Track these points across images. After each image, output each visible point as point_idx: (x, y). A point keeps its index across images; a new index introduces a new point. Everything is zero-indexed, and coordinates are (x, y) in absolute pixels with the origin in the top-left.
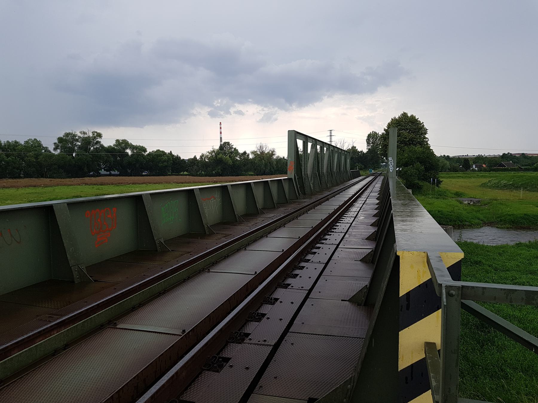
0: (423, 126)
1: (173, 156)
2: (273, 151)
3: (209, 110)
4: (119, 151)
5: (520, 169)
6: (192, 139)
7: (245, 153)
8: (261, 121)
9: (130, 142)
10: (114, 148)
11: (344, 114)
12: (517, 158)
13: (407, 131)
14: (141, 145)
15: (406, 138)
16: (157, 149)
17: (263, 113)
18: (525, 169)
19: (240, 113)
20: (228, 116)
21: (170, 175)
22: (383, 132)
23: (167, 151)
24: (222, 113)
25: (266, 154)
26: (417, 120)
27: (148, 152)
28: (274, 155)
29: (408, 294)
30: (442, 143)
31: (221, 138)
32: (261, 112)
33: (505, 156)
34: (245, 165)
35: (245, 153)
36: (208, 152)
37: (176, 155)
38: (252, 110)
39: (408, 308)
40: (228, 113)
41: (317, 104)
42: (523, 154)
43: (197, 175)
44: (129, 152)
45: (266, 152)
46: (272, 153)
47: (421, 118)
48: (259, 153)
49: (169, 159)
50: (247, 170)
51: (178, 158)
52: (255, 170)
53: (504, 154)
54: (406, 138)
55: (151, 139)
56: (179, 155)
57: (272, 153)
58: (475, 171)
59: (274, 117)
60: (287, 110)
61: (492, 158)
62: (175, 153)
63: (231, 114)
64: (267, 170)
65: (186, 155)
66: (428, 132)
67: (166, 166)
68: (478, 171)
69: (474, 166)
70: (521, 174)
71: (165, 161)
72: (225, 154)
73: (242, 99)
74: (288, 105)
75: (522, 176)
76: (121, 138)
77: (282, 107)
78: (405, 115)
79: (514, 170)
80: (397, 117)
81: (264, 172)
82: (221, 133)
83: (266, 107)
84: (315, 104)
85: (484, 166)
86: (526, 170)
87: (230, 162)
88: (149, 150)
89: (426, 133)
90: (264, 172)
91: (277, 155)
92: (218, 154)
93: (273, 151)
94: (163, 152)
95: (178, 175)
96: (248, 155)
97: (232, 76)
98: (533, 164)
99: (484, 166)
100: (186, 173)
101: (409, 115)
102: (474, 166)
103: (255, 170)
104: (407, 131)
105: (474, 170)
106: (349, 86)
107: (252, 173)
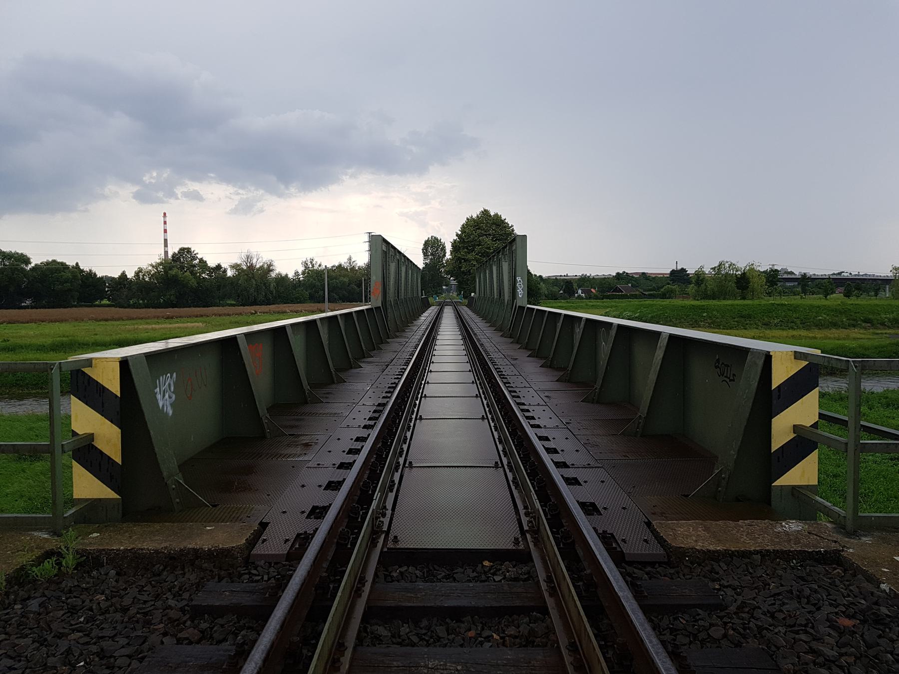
0: (513, 230)
1: (82, 271)
2: (270, 265)
3: (135, 189)
5: (643, 296)
6: (118, 241)
7: (219, 267)
8: (235, 211)
11: (378, 206)
12: (636, 280)
13: (488, 241)
15: (489, 248)
17: (237, 197)
18: (650, 295)
19: (196, 197)
20: (172, 201)
21: (76, 306)
22: (456, 238)
23: (71, 263)
24: (161, 194)
25: (258, 270)
26: (503, 222)
27: (33, 265)
28: (272, 270)
29: (779, 387)
30: (544, 260)
31: (166, 241)
32: (233, 197)
35: (219, 267)
36: (152, 265)
37: (86, 269)
38: (218, 193)
39: (779, 396)
40: (172, 195)
41: (334, 188)
42: (643, 273)
43: (129, 306)
45: (258, 266)
46: (269, 268)
48: (245, 268)
49: (75, 277)
51: (91, 275)
53: (618, 274)
54: (489, 248)
57: (269, 268)
58: (582, 298)
59: (259, 205)
60: (280, 195)
63: (177, 198)
64: (261, 298)
65: (288, 265)
67: (70, 290)
68: (586, 298)
69: (580, 291)
70: (649, 302)
72: (182, 268)
73: (199, 173)
74: (282, 187)
75: (652, 305)
77: (272, 191)
78: (485, 213)
80: (475, 216)
82: (165, 231)
84: (330, 188)
86: (651, 296)
87: (193, 283)
88: (35, 261)
91: (277, 272)
92: (170, 269)
94: (63, 264)
95: (91, 306)
96: (225, 271)
97: (175, 131)
98: (659, 288)
100: (105, 302)
101: (492, 214)
102: (580, 291)
104: (488, 241)
105: (580, 297)
106: (383, 161)
107: (233, 302)
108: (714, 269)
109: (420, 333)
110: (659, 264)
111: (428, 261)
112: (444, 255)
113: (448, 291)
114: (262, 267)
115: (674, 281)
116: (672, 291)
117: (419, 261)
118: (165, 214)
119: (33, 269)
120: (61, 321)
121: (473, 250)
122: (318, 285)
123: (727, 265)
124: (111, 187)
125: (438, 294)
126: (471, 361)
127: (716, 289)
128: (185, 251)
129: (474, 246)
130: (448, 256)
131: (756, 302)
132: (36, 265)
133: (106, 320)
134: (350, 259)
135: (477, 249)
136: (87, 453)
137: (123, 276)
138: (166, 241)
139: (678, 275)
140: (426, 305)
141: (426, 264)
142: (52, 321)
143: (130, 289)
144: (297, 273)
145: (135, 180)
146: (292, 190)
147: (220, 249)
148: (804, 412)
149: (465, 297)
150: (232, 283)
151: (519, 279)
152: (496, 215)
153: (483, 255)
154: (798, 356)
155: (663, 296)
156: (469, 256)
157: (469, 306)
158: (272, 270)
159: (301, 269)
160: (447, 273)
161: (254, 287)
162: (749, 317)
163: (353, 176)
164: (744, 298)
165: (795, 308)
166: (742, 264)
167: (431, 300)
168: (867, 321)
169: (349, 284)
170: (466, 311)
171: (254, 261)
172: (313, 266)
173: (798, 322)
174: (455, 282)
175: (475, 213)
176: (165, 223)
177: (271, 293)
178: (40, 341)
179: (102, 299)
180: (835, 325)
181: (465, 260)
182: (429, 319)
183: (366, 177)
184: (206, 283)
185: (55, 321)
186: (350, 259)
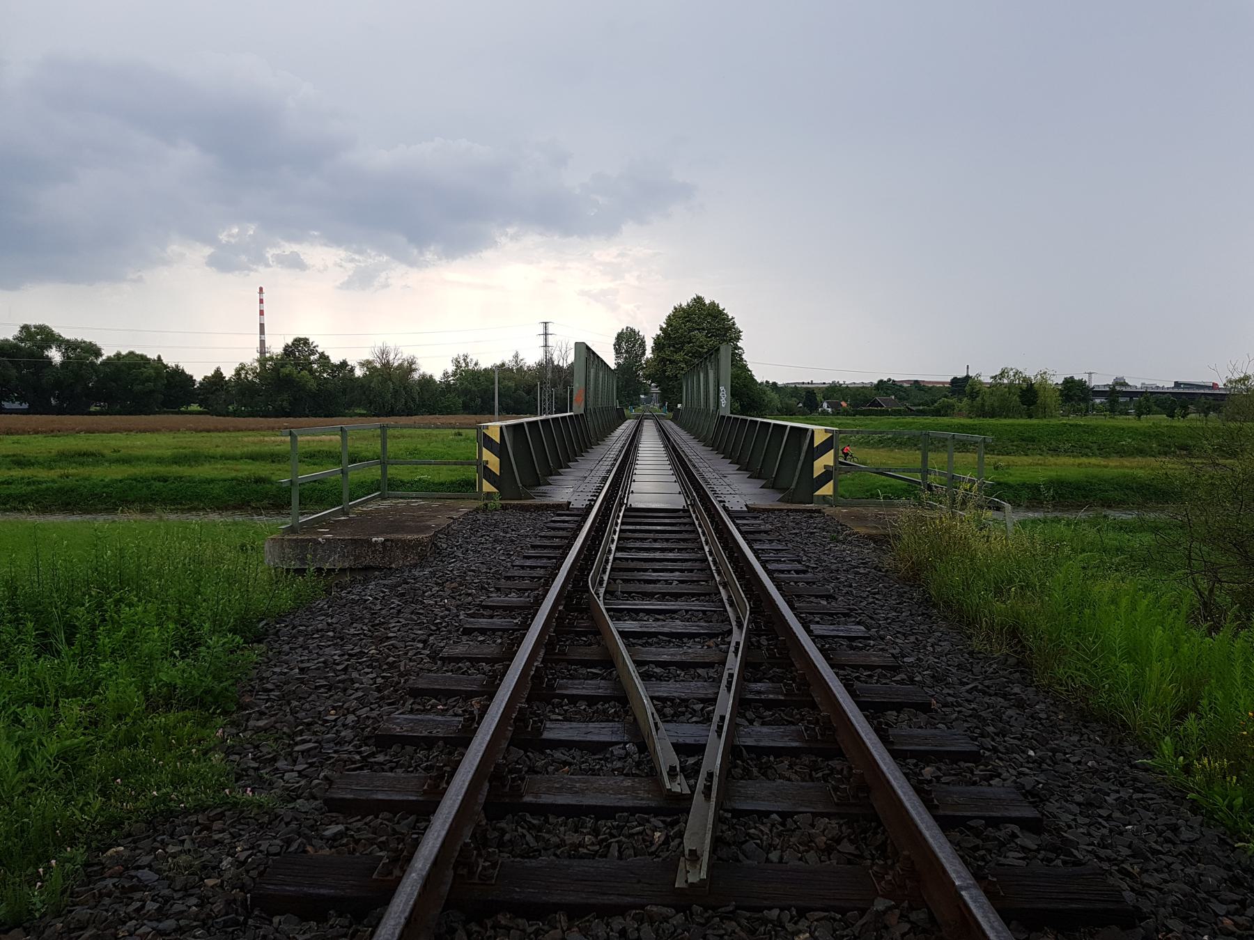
1: (166, 367)
2: (412, 363)
4: (31, 354)
6: (206, 325)
8: (347, 285)
9: (56, 330)
10: (16, 346)
13: (700, 334)
14: (88, 340)
16: (132, 349)
17: (351, 265)
19: (295, 263)
20: (261, 269)
22: (659, 332)
23: (152, 355)
24: (244, 258)
26: (721, 313)
28: (415, 370)
31: (262, 326)
33: (884, 387)
34: (344, 392)
37: (172, 364)
38: (323, 257)
40: (260, 259)
41: (488, 254)
43: (228, 414)
44: (55, 355)
46: (409, 368)
47: (730, 309)
48: (378, 366)
50: (350, 405)
52: (371, 403)
53: (881, 381)
54: (702, 347)
55: (109, 321)
56: (181, 366)
57: (409, 368)
58: (828, 414)
60: (412, 264)
61: (858, 389)
62: (170, 361)
63: (267, 265)
64: (400, 406)
66: (743, 336)
67: (152, 392)
69: (825, 405)
70: (909, 419)
71: (148, 379)
73: (296, 229)
74: (415, 252)
76: (34, 321)
78: (699, 300)
79: (898, 413)
80: (684, 305)
81: (392, 409)
82: (262, 313)
83: (360, 252)
85: (844, 404)
87: (312, 385)
88: (108, 352)
89: (738, 339)
90: (392, 409)
93: (412, 363)
94: (143, 357)
95: (177, 413)
96: (352, 370)
97: (265, 170)
99: (844, 404)
101: (707, 302)
102: (825, 405)
103: (371, 403)
104: (700, 334)
105: (824, 413)
106: (557, 216)
108: (994, 377)
109: (613, 455)
110: (939, 372)
111: (621, 361)
112: (644, 353)
113: (648, 401)
114: (401, 365)
115: (953, 392)
116: (951, 407)
117: (610, 359)
118: (261, 289)
119: (104, 363)
120: (153, 431)
121: (681, 349)
122: (475, 391)
123: (1011, 373)
124: (174, 248)
125: (635, 404)
126: (675, 468)
127: (996, 404)
128: (301, 343)
129: (683, 344)
130: (649, 354)
131: (1045, 421)
132: (109, 358)
133: (208, 431)
134: (516, 356)
135: (687, 347)
136: (487, 474)
137: (218, 374)
138: (262, 326)
139: (961, 386)
140: (622, 419)
141: (618, 365)
142: (141, 431)
143: (228, 392)
144: (445, 374)
145: (210, 240)
146: (429, 256)
147: (349, 343)
148: (828, 459)
149: (670, 409)
150: (362, 386)
151: (722, 388)
152: (713, 304)
153: (694, 356)
154: (826, 431)
155: (937, 413)
156: (677, 357)
157: (674, 419)
158: (415, 370)
159: (451, 368)
160: (647, 377)
161: (390, 392)
162: (1032, 440)
163: (514, 238)
164: (1030, 417)
165: (1091, 430)
166: (1031, 373)
167: (626, 412)
168: (1183, 447)
169: (516, 390)
170: (670, 425)
171: (391, 357)
172: (467, 365)
173: (1095, 447)
174: (657, 390)
175: (685, 301)
176: (261, 301)
177: (413, 400)
178: (157, 452)
179: (189, 405)
180: (1141, 452)
181: (672, 362)
182: (628, 432)
183: (532, 239)
184: (329, 386)
185: (145, 431)
186: (516, 356)
